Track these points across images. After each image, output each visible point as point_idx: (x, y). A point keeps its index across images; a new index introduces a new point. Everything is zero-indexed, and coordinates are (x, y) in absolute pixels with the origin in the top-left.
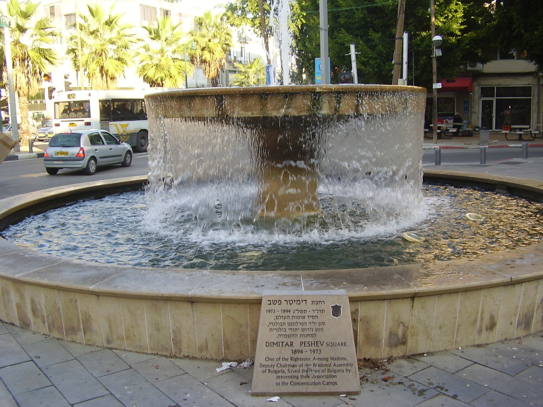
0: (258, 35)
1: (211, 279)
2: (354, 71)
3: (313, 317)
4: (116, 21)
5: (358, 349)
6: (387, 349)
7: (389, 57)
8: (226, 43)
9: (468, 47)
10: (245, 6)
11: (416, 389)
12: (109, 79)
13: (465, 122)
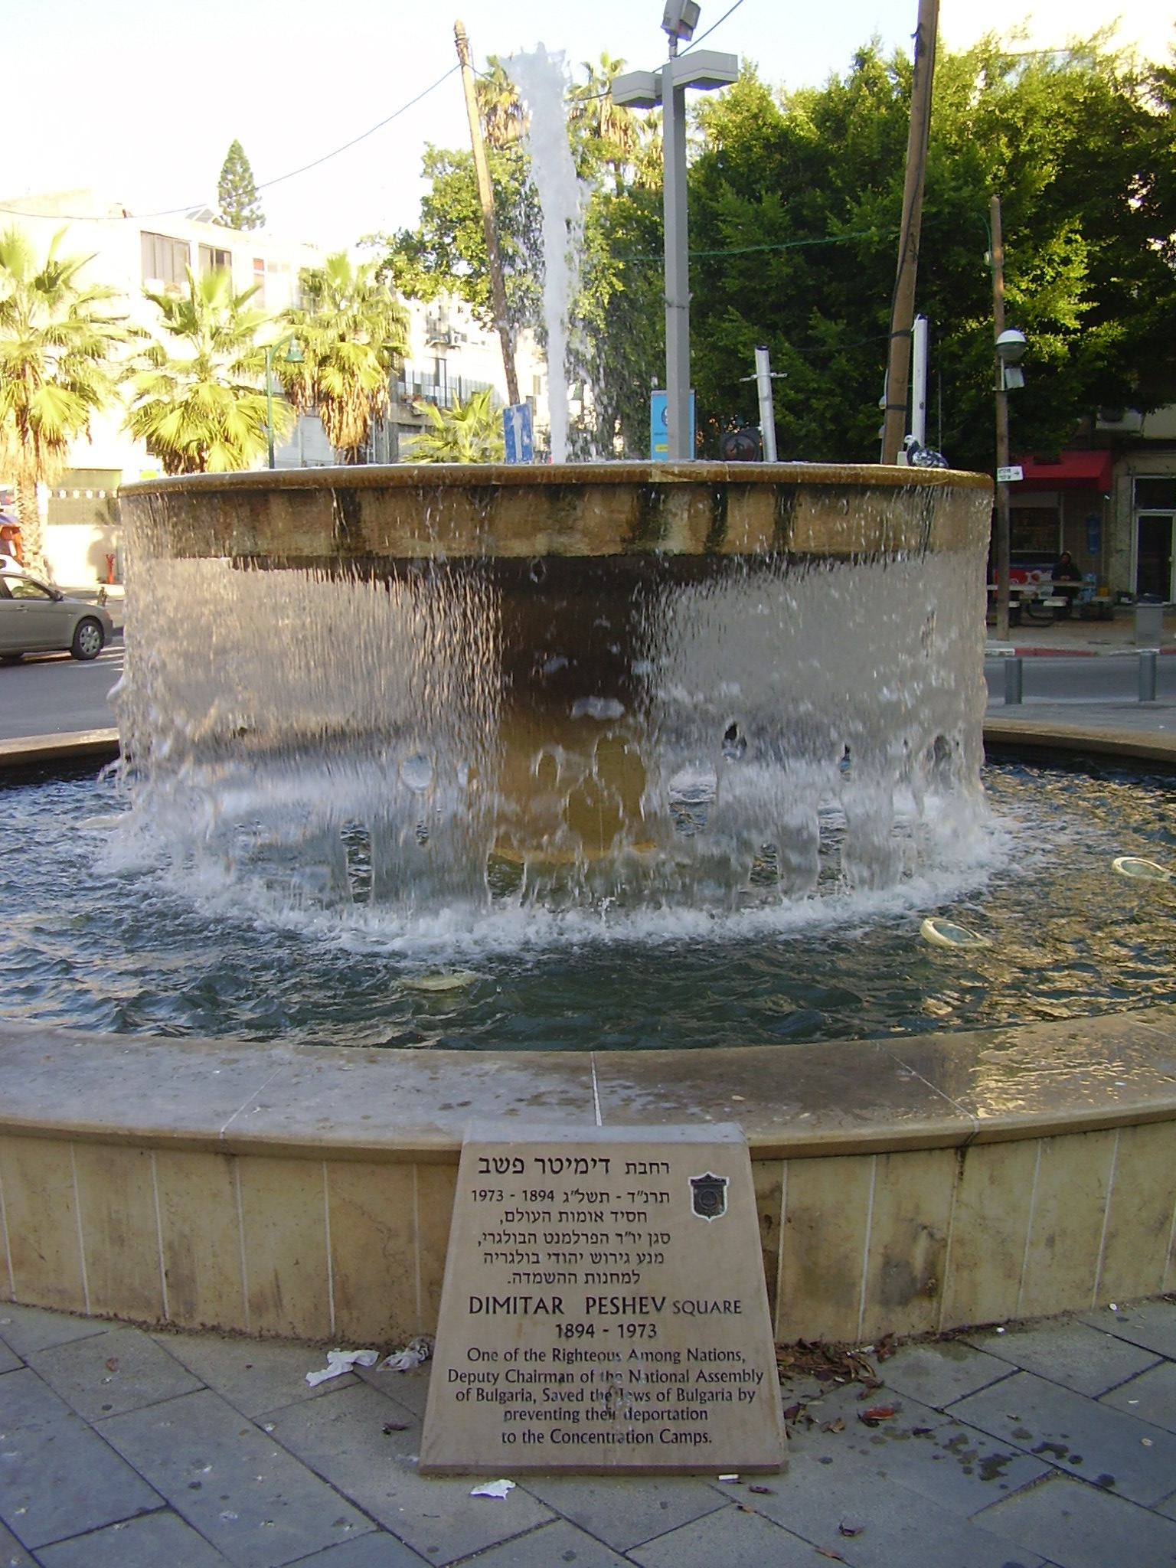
0: (485, 325)
1: (296, 1076)
2: (766, 426)
3: (631, 1217)
4: (68, 278)
5: (778, 1312)
6: (876, 1310)
7: (871, 389)
8: (388, 345)
9: (1100, 364)
10: (447, 240)
11: (974, 1452)
12: (42, 444)
13: (1089, 578)
